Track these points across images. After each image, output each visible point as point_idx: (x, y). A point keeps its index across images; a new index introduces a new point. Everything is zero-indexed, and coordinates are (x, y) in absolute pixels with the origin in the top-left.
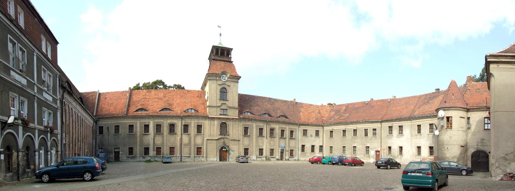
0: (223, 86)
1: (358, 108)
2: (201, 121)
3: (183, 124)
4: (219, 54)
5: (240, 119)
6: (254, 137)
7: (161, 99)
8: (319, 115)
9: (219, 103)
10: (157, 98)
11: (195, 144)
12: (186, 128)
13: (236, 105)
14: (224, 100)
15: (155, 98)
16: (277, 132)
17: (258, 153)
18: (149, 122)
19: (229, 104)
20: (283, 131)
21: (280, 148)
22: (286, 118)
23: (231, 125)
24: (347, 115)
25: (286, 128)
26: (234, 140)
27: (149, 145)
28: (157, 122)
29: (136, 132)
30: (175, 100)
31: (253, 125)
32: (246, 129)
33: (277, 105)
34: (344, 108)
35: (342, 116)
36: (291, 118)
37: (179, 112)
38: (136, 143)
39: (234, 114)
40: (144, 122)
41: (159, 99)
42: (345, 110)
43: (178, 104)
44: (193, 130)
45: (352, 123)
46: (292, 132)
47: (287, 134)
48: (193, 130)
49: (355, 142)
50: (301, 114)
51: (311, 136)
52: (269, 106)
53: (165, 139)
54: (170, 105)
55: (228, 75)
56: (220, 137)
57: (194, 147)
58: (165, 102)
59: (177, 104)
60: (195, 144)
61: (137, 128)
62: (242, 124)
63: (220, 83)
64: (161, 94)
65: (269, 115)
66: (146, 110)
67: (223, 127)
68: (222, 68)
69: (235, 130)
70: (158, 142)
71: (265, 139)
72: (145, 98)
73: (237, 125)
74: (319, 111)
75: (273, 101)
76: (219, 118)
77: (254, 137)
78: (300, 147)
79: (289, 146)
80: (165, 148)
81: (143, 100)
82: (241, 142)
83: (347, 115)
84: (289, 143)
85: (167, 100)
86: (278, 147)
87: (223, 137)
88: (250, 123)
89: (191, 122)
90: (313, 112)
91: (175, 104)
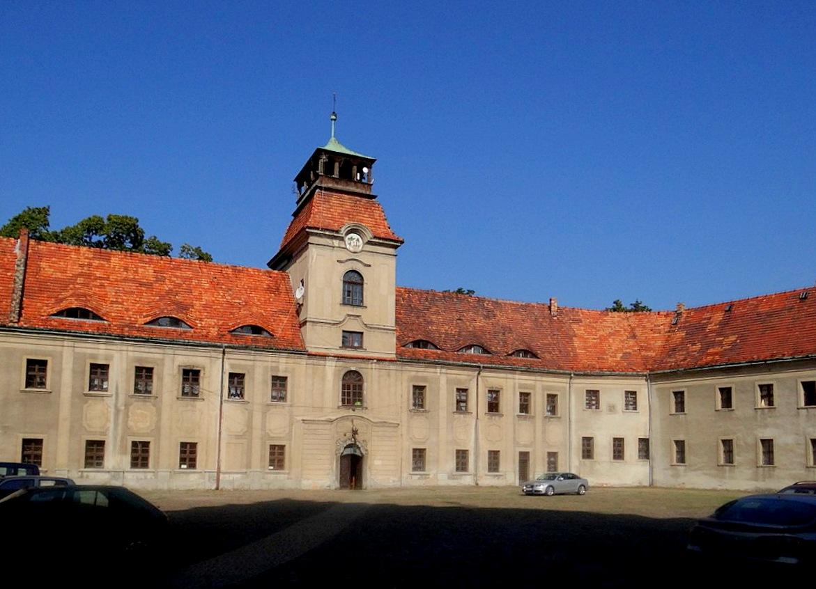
1: (769, 315)
3: (228, 369)
5: (402, 359)
7: (149, 285)
8: (632, 342)
10: (134, 280)
11: (265, 436)
13: (391, 321)
15: (126, 280)
16: (509, 402)
17: (452, 464)
18: (110, 357)
19: (368, 315)
20: (525, 396)
21: (289, 402)
22: (534, 355)
24: (733, 338)
25: (534, 387)
27: (104, 434)
28: (140, 360)
29: (58, 384)
33: (501, 318)
34: (718, 317)
35: (713, 344)
36: (548, 356)
38: (53, 425)
39: (382, 344)
40: (93, 356)
41: (141, 284)
42: (724, 324)
45: (752, 368)
46: (552, 399)
47: (538, 403)
49: (766, 426)
50: (577, 342)
51: (612, 409)
52: (480, 322)
53: (165, 416)
54: (184, 308)
57: (263, 444)
58: (162, 297)
59: (205, 306)
60: (265, 436)
61: (59, 373)
63: (344, 256)
64: (145, 267)
66: (96, 317)
69: (387, 389)
70: (140, 425)
72: (88, 276)
74: (633, 329)
75: (490, 306)
76: (339, 357)
78: (576, 444)
80: (164, 443)
81: (80, 280)
83: (733, 338)
84: (544, 432)
85: (170, 292)
90: (611, 335)
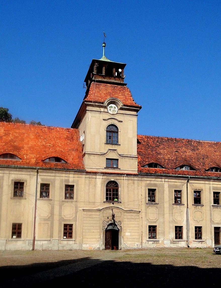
0: (111, 122)
2: (72, 178)
3: (40, 181)
4: (104, 73)
5: (141, 174)
6: (167, 205)
9: (105, 148)
11: (61, 219)
12: (45, 189)
14: (112, 144)
17: (173, 235)
23: (126, 188)
26: (131, 211)
30: (26, 141)
31: (163, 186)
32: (152, 193)
37: (33, 161)
43: (32, 149)
44: (57, 192)
48: (57, 192)
52: (189, 153)
54: (18, 149)
55: (121, 105)
56: (107, 205)
57: (60, 223)
59: (30, 148)
62: (144, 183)
63: (107, 116)
65: (192, 168)
67: (112, 192)
68: (109, 94)
69: (133, 192)
71: (184, 209)
73: (136, 185)
77: (167, 205)
79: (60, 214)
82: (143, 214)
86: (209, 222)
87: (111, 205)
88: (158, 181)
89: (54, 180)
91: (26, 147)
